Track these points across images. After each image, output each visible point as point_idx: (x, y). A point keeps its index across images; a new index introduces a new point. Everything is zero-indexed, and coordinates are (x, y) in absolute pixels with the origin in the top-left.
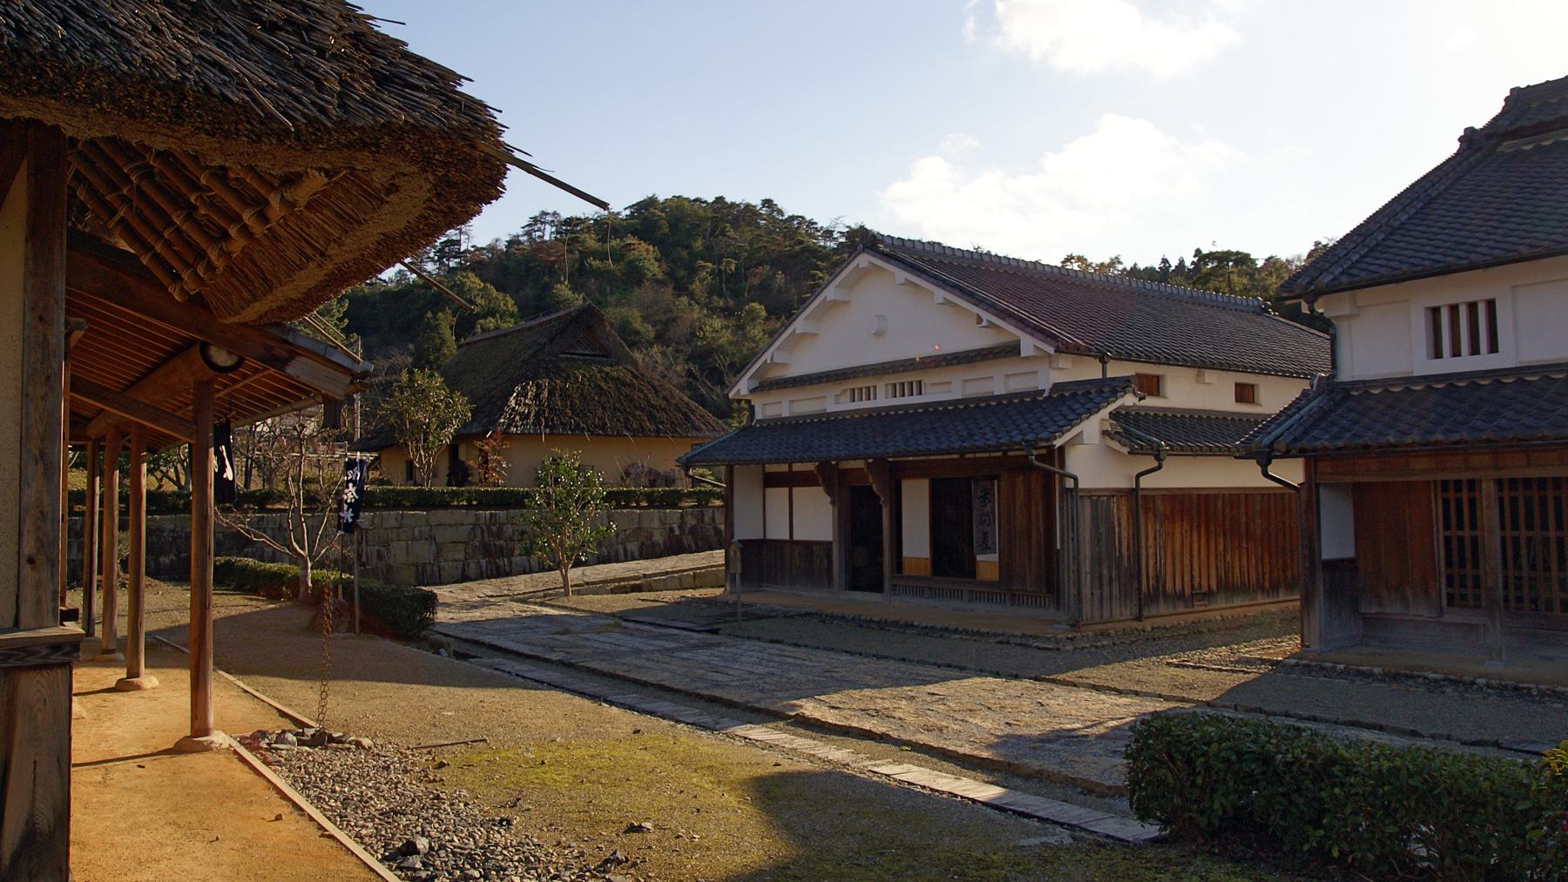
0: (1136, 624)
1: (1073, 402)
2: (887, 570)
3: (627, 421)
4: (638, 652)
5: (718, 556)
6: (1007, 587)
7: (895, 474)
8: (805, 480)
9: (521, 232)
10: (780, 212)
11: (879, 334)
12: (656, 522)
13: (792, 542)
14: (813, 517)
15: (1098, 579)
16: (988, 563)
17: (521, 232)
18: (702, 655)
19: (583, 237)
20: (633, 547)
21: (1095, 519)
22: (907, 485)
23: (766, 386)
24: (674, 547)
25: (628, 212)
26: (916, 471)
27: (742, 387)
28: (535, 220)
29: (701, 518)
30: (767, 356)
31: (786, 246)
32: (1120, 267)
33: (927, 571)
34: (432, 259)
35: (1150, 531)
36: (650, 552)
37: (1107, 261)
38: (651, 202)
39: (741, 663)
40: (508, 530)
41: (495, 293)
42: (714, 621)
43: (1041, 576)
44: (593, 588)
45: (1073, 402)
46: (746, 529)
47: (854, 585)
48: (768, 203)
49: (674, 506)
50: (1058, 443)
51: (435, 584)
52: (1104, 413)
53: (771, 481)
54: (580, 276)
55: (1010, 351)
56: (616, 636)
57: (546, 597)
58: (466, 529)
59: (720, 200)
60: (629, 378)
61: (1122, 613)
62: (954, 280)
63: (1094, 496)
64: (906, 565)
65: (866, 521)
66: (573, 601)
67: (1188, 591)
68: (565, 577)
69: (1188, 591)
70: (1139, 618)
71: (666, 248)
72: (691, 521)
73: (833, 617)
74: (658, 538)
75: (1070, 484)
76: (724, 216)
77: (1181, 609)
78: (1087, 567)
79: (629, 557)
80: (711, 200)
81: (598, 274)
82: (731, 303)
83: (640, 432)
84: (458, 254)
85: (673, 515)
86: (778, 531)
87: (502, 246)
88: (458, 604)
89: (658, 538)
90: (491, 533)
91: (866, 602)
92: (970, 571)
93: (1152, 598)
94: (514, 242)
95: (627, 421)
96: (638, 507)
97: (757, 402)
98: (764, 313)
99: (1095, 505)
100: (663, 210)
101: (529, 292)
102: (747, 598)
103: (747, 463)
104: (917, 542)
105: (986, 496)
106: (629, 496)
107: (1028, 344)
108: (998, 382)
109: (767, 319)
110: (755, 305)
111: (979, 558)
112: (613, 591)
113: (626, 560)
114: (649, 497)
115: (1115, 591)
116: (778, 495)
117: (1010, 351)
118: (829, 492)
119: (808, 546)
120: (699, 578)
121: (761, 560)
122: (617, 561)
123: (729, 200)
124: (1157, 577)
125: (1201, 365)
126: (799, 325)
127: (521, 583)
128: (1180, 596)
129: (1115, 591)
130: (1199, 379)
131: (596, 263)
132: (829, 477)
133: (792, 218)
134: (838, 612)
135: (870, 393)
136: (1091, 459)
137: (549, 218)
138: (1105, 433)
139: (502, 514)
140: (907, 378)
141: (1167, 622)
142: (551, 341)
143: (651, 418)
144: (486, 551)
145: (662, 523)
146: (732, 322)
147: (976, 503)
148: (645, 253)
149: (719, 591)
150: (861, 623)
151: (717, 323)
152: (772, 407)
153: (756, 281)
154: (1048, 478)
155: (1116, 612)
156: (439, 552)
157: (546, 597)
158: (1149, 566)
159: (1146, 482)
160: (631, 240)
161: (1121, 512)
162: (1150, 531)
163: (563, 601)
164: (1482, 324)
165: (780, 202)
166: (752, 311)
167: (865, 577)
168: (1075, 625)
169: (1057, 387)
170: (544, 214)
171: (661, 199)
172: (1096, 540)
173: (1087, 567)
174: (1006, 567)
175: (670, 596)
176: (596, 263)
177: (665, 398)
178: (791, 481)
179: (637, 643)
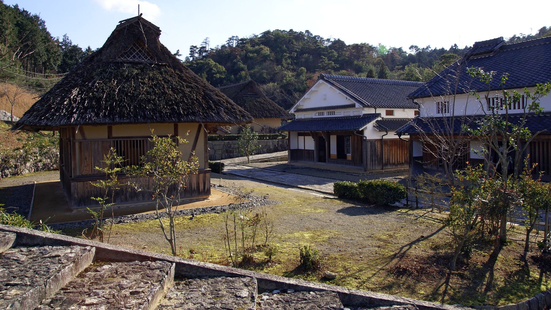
0: (381, 171)
1: (368, 118)
2: (327, 157)
3: (263, 114)
4: (267, 176)
5: (285, 153)
6: (353, 162)
7: (329, 134)
8: (308, 135)
9: (226, 43)
10: (311, 34)
11: (325, 99)
12: (271, 143)
13: (305, 150)
14: (309, 144)
15: (372, 160)
16: (349, 156)
17: (226, 43)
18: (280, 176)
19: (246, 45)
20: (265, 150)
21: (371, 147)
22: (332, 137)
23: (298, 110)
24: (276, 150)
25: (261, 35)
26: (333, 134)
27: (292, 111)
28: (230, 39)
29: (283, 142)
30: (298, 103)
31: (313, 47)
32: (430, 49)
33: (336, 157)
34: (197, 53)
35: (386, 149)
36: (269, 151)
37: (425, 47)
38: (268, 33)
39: (289, 177)
40: (232, 146)
41: (219, 66)
42: (283, 169)
43: (359, 160)
44: (257, 160)
45: (368, 118)
46: (293, 146)
47: (320, 160)
48: (307, 31)
49: (276, 139)
50: (360, 130)
51: (222, 159)
52: (374, 121)
53: (300, 134)
54: (246, 59)
55: (353, 106)
56: (262, 173)
57: (243, 164)
58: (222, 146)
59: (291, 30)
60: (263, 101)
61: (378, 168)
62: (342, 87)
63: (373, 142)
64: (331, 156)
65: (322, 145)
66: (250, 164)
67: (396, 163)
68: (248, 159)
69: (396, 163)
70: (382, 169)
71: (272, 49)
72: (280, 143)
73: (312, 168)
74: (272, 147)
75: (365, 138)
76: (294, 37)
77: (394, 167)
78: (369, 157)
79: (264, 153)
80: (288, 31)
81: (251, 58)
82: (295, 67)
83: (266, 117)
84: (206, 51)
85: (276, 141)
86: (301, 147)
87: (220, 48)
88: (229, 165)
89: (272, 147)
90: (228, 147)
91: (322, 165)
92: (345, 157)
93: (386, 164)
94: (223, 47)
95: (263, 114)
96: (266, 139)
97: (296, 114)
98: (306, 71)
99: (371, 144)
100: (272, 35)
101: (229, 64)
102: (293, 164)
103: (293, 131)
104: (334, 151)
105: (348, 140)
106: (263, 136)
107: (357, 105)
108: (350, 113)
109: (307, 72)
110: (303, 68)
111: (60, 180)
112: (260, 162)
113: (263, 153)
114: (269, 136)
115: (376, 163)
116: (301, 138)
117: (353, 106)
118: (313, 138)
119: (308, 151)
120: (282, 159)
121: (296, 154)
122: (261, 154)
123: (294, 30)
124: (388, 160)
125: (404, 107)
126: (306, 96)
127: (237, 160)
128: (394, 164)
129: (376, 163)
130: (404, 111)
131: (251, 55)
132: (314, 135)
133: (316, 36)
134: (314, 167)
135: (323, 114)
136: (370, 132)
137: (235, 38)
138: (374, 126)
139: (231, 142)
140: (331, 111)
141: (389, 170)
142: (241, 91)
143: (269, 112)
144: (227, 151)
145: (273, 143)
146: (295, 73)
147: (346, 142)
148: (266, 50)
149: (287, 162)
150: (318, 170)
151: (290, 74)
152: (300, 116)
153: (303, 60)
154: (362, 137)
155: (377, 168)
156: (215, 152)
157: (243, 164)
158: (385, 157)
159: (384, 137)
160: (262, 46)
161: (378, 145)
162: (386, 149)
163: (248, 165)
164: (442, 107)
165: (311, 31)
166: (302, 70)
167: (322, 159)
168: (365, 171)
169: (364, 115)
170: (233, 37)
171: (272, 31)
172: (371, 151)
173: (369, 157)
174: (353, 157)
175: (275, 163)
176: (251, 55)
177: (273, 107)
178: (304, 135)
179: (267, 174)
